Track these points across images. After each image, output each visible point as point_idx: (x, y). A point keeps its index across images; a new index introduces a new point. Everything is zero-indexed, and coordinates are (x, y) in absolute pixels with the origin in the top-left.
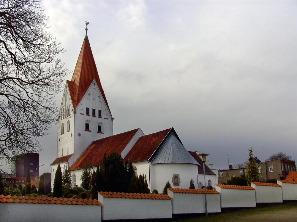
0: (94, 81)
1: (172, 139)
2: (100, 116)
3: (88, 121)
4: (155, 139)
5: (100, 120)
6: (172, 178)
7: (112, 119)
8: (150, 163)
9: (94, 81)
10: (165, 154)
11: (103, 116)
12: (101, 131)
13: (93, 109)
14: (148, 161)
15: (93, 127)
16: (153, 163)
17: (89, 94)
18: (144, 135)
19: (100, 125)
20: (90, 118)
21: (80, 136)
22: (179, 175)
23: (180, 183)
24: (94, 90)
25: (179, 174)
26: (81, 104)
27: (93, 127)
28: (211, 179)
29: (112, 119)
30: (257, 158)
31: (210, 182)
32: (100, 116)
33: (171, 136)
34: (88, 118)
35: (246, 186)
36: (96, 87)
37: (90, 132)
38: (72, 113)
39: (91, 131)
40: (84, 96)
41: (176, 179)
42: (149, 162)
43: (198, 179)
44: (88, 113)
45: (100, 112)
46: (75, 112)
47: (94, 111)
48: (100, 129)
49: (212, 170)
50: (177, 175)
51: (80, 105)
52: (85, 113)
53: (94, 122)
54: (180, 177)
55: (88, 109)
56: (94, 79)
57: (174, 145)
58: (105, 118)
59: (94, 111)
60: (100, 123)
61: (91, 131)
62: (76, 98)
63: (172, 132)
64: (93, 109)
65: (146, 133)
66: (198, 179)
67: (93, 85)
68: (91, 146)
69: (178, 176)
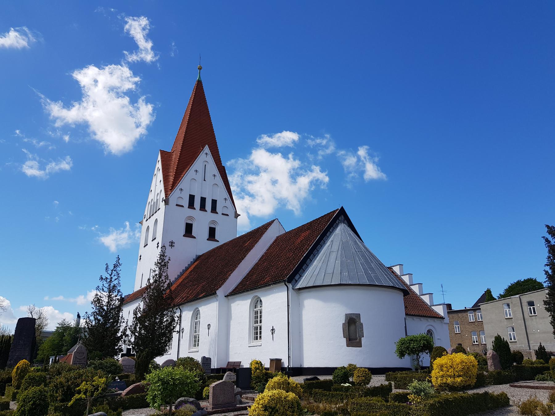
0: (207, 149)
1: (341, 229)
2: (192, 198)
3: (190, 218)
5: (213, 216)
6: (343, 324)
7: (237, 215)
8: (290, 286)
9: (207, 149)
11: (219, 208)
14: (285, 281)
15: (201, 231)
16: (298, 287)
19: (213, 226)
20: (196, 213)
22: (358, 316)
24: (206, 163)
27: (201, 231)
29: (237, 215)
32: (214, 209)
34: (190, 212)
35: (272, 378)
36: (210, 159)
38: (162, 205)
39: (195, 238)
41: (352, 327)
42: (286, 283)
43: (406, 327)
44: (191, 205)
45: (214, 202)
46: (166, 202)
47: (203, 200)
48: (212, 232)
50: (354, 317)
52: (186, 203)
53: (202, 221)
54: (362, 321)
55: (192, 198)
56: (207, 146)
58: (223, 214)
59: (203, 200)
60: (214, 222)
61: (195, 238)
62: (171, 179)
63: (342, 212)
66: (406, 327)
68: (192, 263)
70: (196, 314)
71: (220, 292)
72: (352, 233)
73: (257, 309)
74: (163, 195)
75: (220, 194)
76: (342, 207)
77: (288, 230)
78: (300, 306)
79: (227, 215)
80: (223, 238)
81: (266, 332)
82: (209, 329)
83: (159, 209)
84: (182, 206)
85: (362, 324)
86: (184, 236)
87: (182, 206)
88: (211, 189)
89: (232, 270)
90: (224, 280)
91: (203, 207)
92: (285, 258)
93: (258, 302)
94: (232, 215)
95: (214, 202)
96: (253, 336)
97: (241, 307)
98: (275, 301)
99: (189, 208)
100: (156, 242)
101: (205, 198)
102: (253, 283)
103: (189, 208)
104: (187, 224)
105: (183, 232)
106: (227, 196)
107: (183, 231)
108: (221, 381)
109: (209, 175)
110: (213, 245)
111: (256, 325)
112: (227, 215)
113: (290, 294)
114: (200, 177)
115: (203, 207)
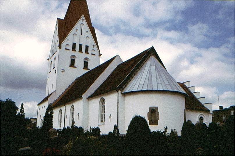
0: (83, 17)
2: (74, 45)
4: (131, 63)
5: (87, 56)
7: (100, 55)
9: (83, 17)
10: (140, 79)
11: (90, 51)
12: (87, 67)
13: (80, 45)
16: (123, 92)
17: (77, 29)
18: (122, 62)
20: (76, 53)
21: (62, 70)
23: (158, 120)
24: (83, 25)
25: (157, 107)
26: (67, 39)
28: (203, 116)
29: (100, 55)
30: (159, 119)
31: (202, 119)
32: (87, 51)
33: (150, 57)
34: (74, 53)
36: (85, 22)
37: (75, 68)
38: (57, 49)
39: (76, 67)
40: (71, 31)
41: (153, 116)
45: (87, 47)
47: (81, 46)
49: (204, 105)
50: (155, 109)
51: (66, 40)
52: (71, 47)
55: (74, 45)
56: (83, 15)
57: (153, 68)
58: (92, 54)
59: (81, 46)
61: (76, 67)
64: (80, 45)
65: (124, 60)
67: (81, 20)
69: (156, 110)
70: (73, 108)
71: (84, 96)
72: (160, 64)
73: (103, 105)
74: (58, 43)
75: (90, 42)
76: (153, 46)
77: (124, 61)
78: (88, 108)
79: (95, 55)
80: (91, 66)
81: (107, 118)
82: (78, 116)
83: (56, 51)
84: (69, 50)
85: (158, 113)
86: (83, 68)
87: (69, 50)
88: (86, 40)
89: (91, 84)
90: (86, 89)
91: (80, 50)
92: (120, 77)
93: (103, 101)
94: (97, 54)
95: (87, 47)
96: (100, 119)
97: (96, 103)
98: (111, 99)
99: (85, 53)
100: (55, 69)
101: (75, 44)
102: (101, 92)
103: (72, 50)
104: (85, 62)
105: (83, 66)
106: (94, 43)
107: (69, 63)
108: (148, 122)
109: (84, 32)
110: (86, 71)
111: (103, 114)
112: (95, 55)
113: (119, 96)
114: (79, 33)
115: (80, 50)
